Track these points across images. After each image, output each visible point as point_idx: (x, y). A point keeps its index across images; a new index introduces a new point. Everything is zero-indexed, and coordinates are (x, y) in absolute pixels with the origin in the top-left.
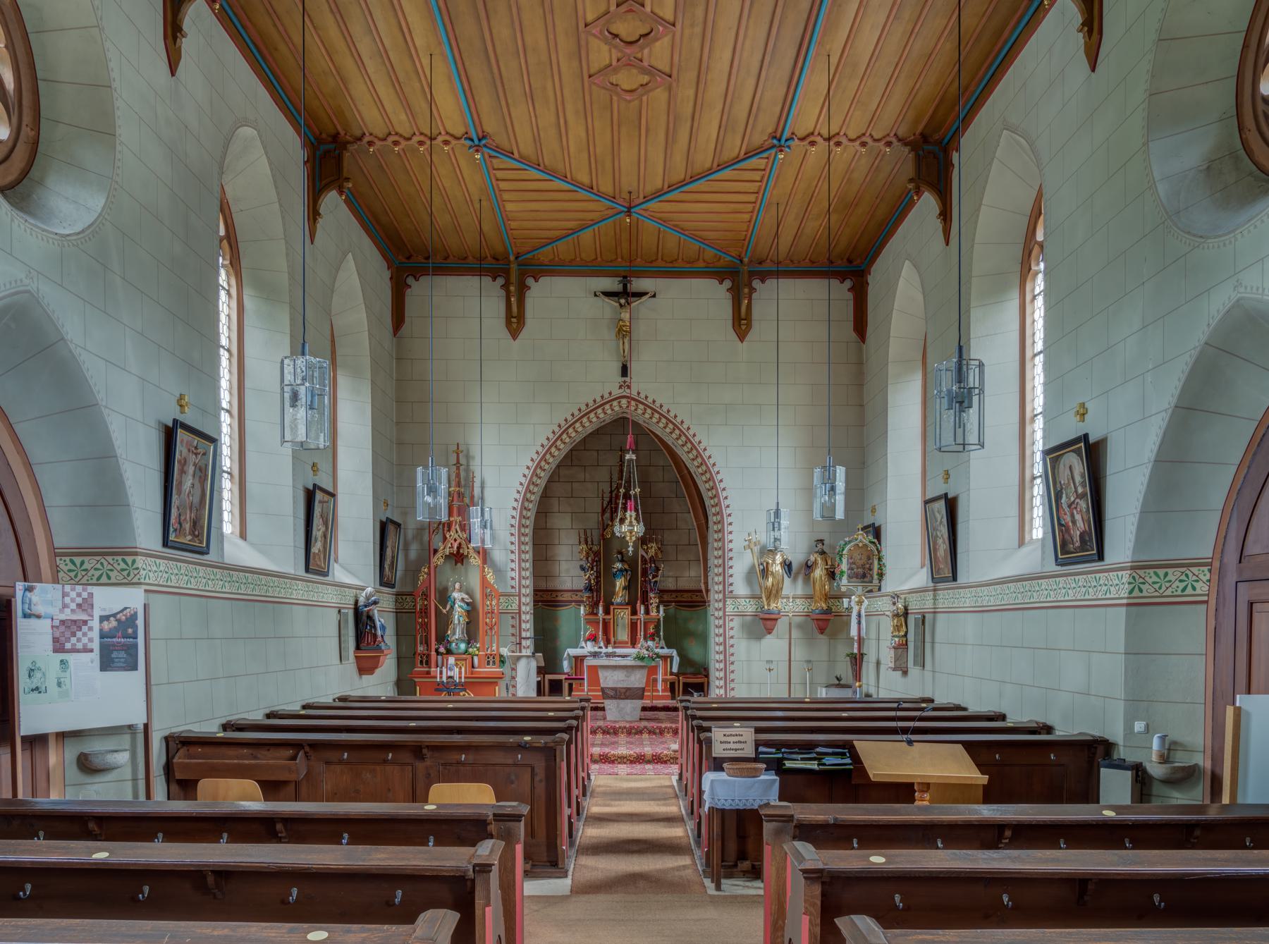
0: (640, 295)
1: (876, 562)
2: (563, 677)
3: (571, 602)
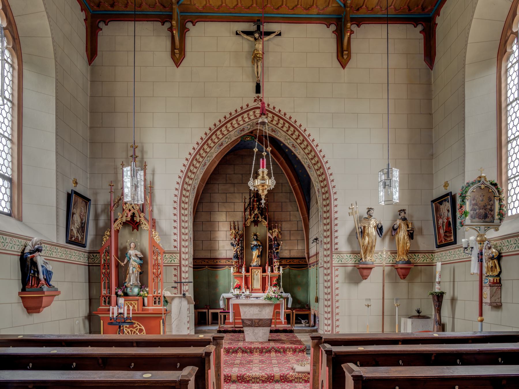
0: (268, 34)
1: (497, 203)
2: (218, 311)
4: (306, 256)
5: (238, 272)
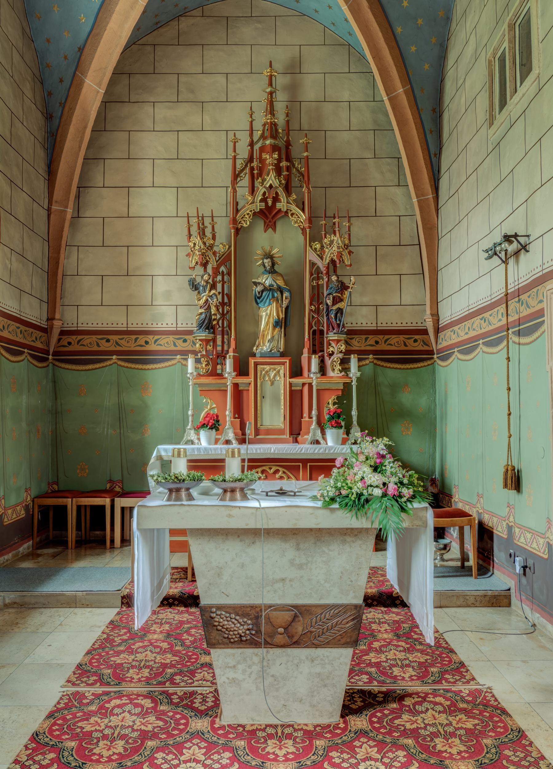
3: (175, 353)
4: (429, 325)
5: (213, 373)
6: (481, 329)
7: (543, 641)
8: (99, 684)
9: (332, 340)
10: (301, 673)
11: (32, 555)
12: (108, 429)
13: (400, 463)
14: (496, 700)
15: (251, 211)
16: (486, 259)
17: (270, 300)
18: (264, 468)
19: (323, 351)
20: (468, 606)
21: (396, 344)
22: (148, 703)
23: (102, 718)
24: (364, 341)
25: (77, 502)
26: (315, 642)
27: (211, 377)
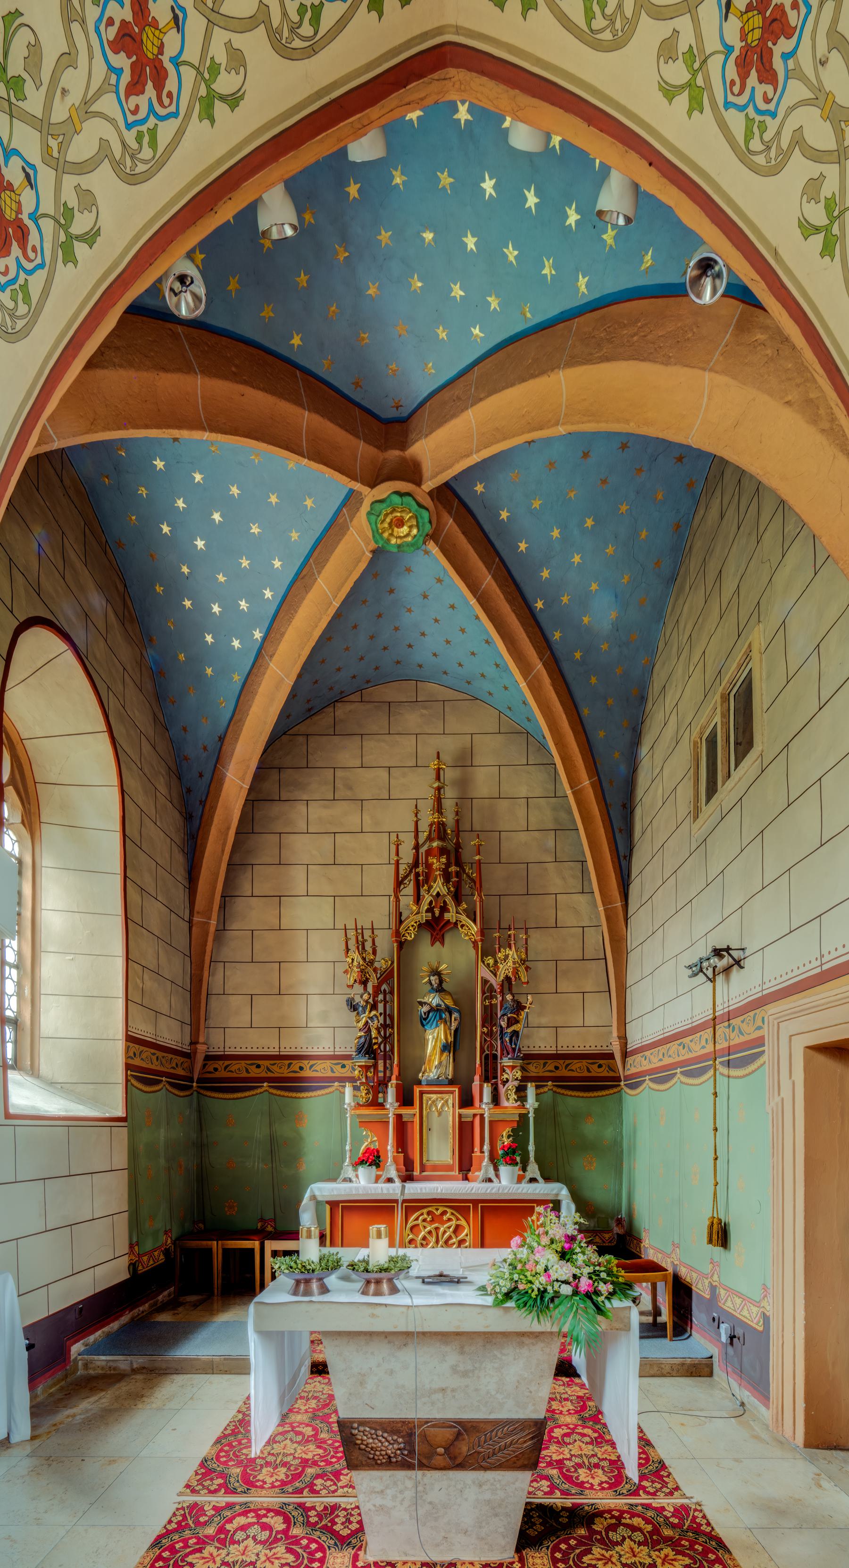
4: (616, 1049)
5: (375, 1104)
6: (679, 1056)
7: (756, 1428)
8: (223, 1490)
9: (506, 1066)
10: (466, 1500)
11: (171, 1305)
12: (258, 1163)
13: (595, 1247)
14: (708, 1524)
15: (416, 922)
16: (690, 977)
17: (437, 1022)
18: (430, 1209)
19: (496, 1078)
20: (663, 1376)
21: (578, 1070)
22: (278, 1523)
23: (219, 1549)
24: (542, 1066)
25: (222, 1245)
26: (483, 1464)
27: (372, 1108)
